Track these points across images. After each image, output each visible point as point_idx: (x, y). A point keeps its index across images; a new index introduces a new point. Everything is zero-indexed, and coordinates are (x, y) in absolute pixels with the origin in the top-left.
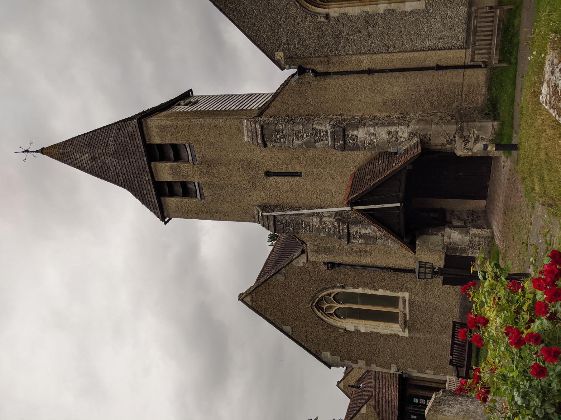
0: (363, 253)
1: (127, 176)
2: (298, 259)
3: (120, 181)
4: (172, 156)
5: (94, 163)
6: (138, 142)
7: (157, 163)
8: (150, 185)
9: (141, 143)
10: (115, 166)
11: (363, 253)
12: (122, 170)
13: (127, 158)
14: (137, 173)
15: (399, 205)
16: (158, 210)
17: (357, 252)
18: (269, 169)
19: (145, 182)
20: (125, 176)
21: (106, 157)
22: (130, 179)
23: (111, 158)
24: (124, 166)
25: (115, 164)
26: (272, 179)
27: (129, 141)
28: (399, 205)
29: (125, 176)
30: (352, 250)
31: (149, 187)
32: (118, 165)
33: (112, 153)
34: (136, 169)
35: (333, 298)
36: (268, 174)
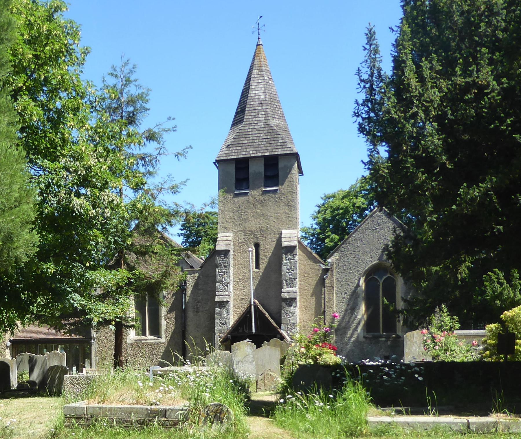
0: (196, 310)
1: (250, 133)
2: (185, 263)
3: (245, 125)
4: (269, 174)
5: (257, 102)
6: (280, 150)
7: (263, 162)
8: (246, 154)
9: (279, 153)
10: (257, 123)
11: (196, 310)
12: (255, 130)
13: (266, 137)
14: (255, 144)
15: (254, 331)
16: (225, 158)
17: (197, 306)
18: (261, 247)
19: (248, 150)
20: (250, 132)
21: (264, 116)
22: (248, 136)
23: (264, 121)
24: (259, 132)
25: (259, 124)
26: (252, 249)
27: (280, 141)
28: (254, 331)
29: (250, 132)
30: (198, 302)
31: (244, 153)
32: (259, 127)
33: (268, 123)
34: (257, 143)
35: (389, 276)
36: (257, 246)
